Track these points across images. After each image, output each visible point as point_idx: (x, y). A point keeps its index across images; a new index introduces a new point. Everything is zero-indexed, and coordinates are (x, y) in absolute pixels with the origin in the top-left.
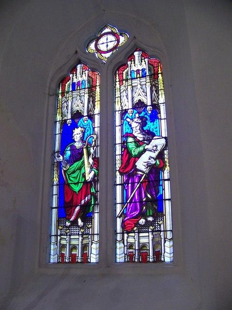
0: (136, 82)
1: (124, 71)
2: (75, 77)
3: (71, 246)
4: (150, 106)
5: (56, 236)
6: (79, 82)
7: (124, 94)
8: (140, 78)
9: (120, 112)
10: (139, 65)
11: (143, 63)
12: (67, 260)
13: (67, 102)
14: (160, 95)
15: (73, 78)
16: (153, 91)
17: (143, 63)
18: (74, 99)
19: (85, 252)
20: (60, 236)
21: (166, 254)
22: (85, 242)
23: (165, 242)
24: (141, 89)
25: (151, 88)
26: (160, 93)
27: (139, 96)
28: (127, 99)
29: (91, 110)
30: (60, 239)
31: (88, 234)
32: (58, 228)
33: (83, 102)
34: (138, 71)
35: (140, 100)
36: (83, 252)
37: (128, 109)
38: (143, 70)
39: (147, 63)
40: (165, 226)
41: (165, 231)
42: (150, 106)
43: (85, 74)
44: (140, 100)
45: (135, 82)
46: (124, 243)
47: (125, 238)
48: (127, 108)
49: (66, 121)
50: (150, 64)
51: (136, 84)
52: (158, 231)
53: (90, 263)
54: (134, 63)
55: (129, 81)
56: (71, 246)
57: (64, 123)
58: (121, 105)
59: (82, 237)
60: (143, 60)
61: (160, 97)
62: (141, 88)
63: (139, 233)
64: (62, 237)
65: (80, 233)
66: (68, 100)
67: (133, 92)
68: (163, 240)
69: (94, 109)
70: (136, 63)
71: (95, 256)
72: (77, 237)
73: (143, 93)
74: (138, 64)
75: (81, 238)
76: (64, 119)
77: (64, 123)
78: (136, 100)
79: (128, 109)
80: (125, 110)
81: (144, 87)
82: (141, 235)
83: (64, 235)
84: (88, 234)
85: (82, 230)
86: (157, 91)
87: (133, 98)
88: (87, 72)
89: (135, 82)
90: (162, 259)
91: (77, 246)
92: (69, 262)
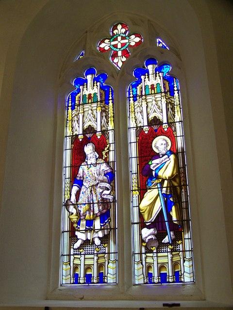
0: (150, 98)
1: (138, 86)
2: (85, 89)
3: (147, 264)
4: (165, 123)
5: (141, 254)
6: (90, 95)
7: (76, 118)
8: (91, 103)
9: (70, 137)
10: (153, 80)
11: (158, 77)
12: (155, 280)
13: (77, 115)
14: (176, 112)
15: (145, 81)
16: (169, 108)
17: (158, 77)
18: (86, 114)
19: (176, 270)
20: (145, 253)
21: (109, 275)
22: (101, 261)
23: (184, 261)
24: (92, 115)
25: (167, 104)
26: (109, 120)
27: (90, 122)
28: (79, 124)
29: (104, 126)
30: (146, 258)
31: (105, 253)
32: (142, 245)
33: (161, 108)
34: (153, 87)
35: (155, 117)
36: (99, 271)
37: (143, 126)
38: (95, 94)
39: (161, 78)
40: (184, 247)
41: (184, 251)
42: (165, 123)
43: (97, 85)
44: (155, 117)
45: (87, 106)
46: (142, 263)
47: (72, 260)
48: (78, 133)
49: (77, 136)
50: (165, 80)
51: (87, 109)
52: (103, 253)
53: (107, 283)
54: (148, 78)
55: (144, 97)
56: (159, 265)
57: (75, 138)
58: (136, 122)
59: (97, 256)
60: (158, 75)
61: (176, 114)
62: (157, 104)
63: (157, 253)
64: (75, 256)
65: (169, 251)
66: (78, 114)
67: (149, 106)
68: (182, 260)
69: (174, 116)
70: (150, 78)
71: (189, 275)
72: (92, 256)
73: (93, 119)
74: (153, 79)
75: (170, 256)
76: (74, 134)
77: (139, 130)
78: (151, 117)
79: (143, 126)
80: (140, 127)
81: (159, 103)
82: (159, 254)
83: (78, 255)
84: (105, 253)
85: (97, 249)
86: (173, 109)
87: (148, 115)
88: (98, 84)
89: (87, 106)
90: (106, 281)
91: (179, 262)
92: (159, 283)
